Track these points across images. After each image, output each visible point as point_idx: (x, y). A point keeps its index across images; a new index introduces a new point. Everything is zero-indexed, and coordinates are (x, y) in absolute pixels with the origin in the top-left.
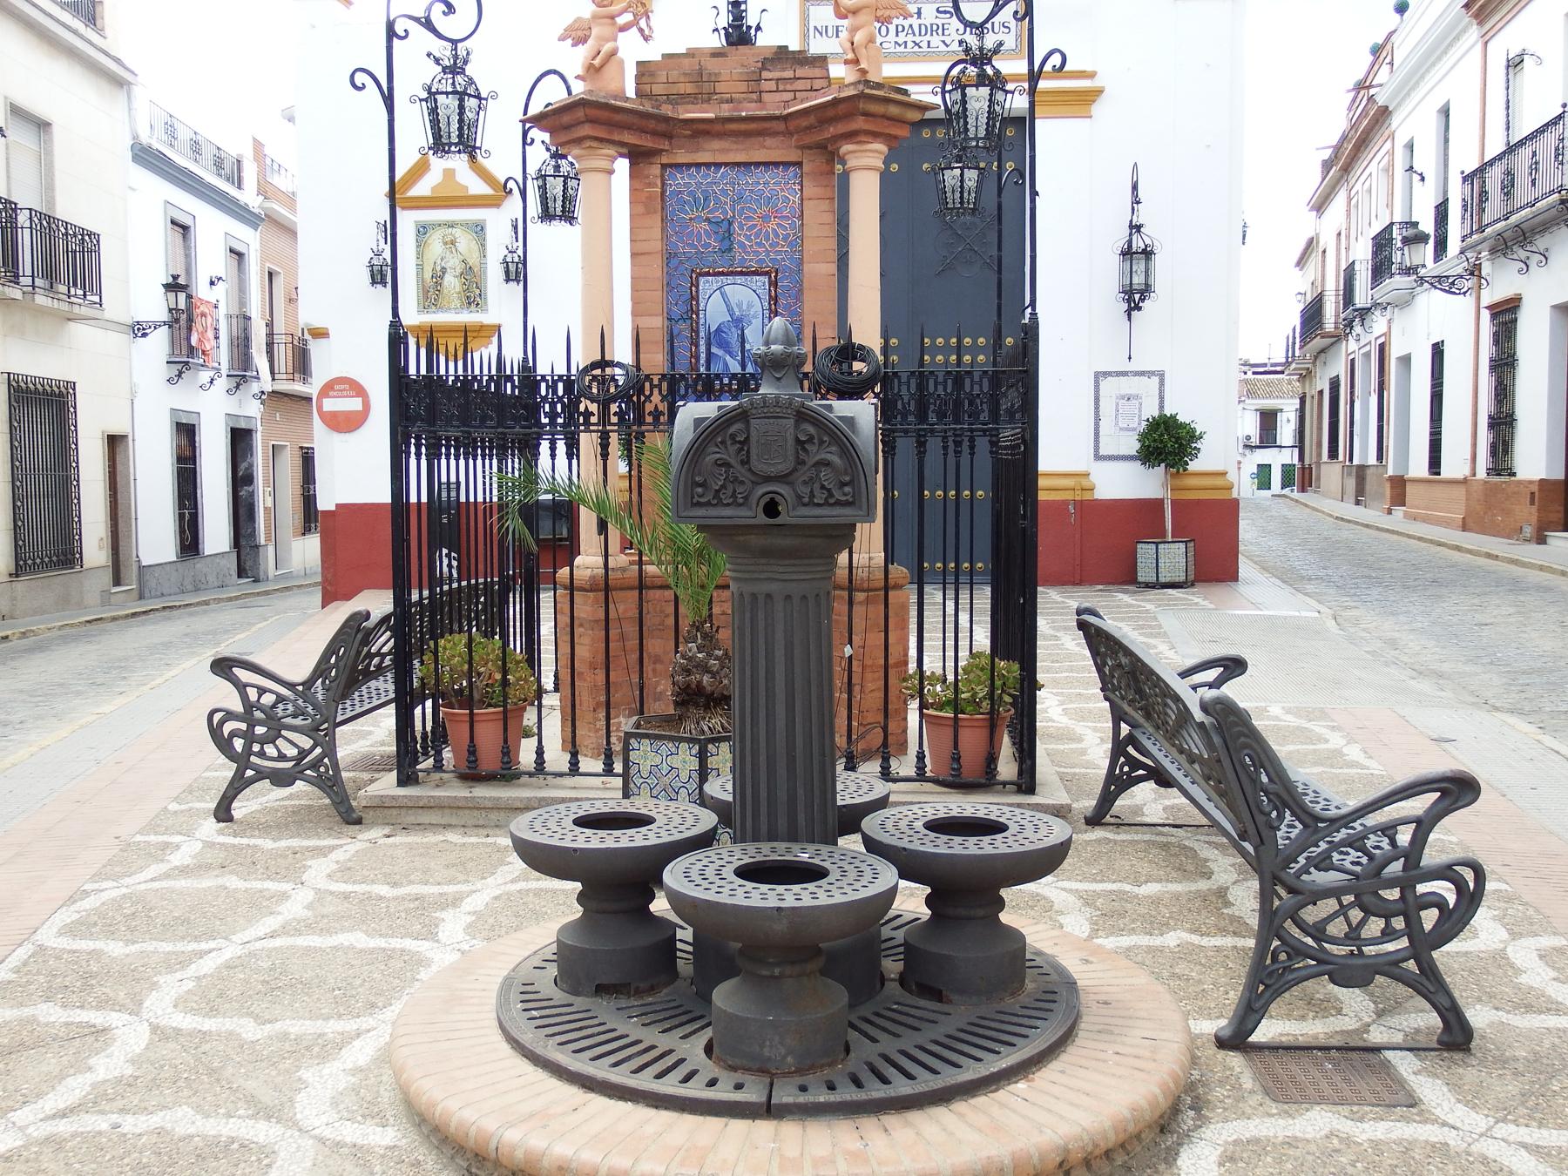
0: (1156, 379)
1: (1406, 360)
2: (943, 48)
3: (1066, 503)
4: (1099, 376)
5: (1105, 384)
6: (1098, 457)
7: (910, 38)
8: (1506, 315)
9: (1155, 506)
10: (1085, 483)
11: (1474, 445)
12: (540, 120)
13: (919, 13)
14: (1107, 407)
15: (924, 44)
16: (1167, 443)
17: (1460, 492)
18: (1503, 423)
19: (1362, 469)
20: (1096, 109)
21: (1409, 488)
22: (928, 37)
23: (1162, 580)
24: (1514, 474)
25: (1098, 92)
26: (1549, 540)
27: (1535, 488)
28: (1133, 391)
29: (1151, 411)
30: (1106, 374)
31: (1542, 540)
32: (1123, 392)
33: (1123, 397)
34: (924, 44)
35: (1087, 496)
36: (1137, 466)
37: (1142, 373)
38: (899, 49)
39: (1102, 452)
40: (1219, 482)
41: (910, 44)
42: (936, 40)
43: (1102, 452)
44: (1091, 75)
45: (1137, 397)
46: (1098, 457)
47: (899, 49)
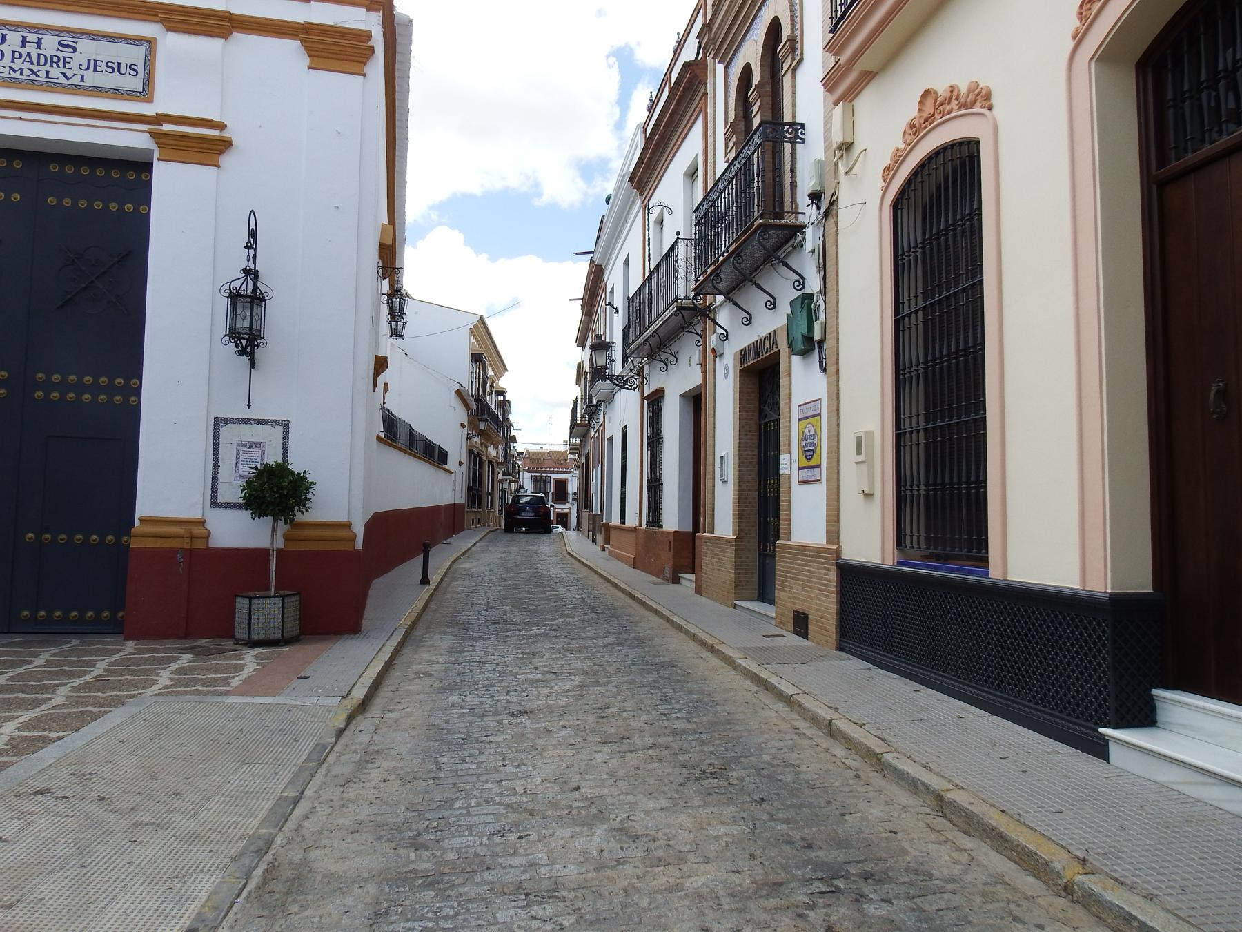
0: (280, 429)
1: (611, 439)
2: (62, 80)
3: (174, 551)
4: (219, 422)
5: (226, 432)
6: (215, 504)
7: (27, 65)
8: (655, 401)
9: (259, 556)
10: (197, 530)
11: (1103, 478)
12: (647, 398)
13: (39, 44)
14: (227, 454)
15: (42, 74)
16: (276, 491)
17: (633, 536)
18: (654, 486)
19: (595, 515)
20: (226, 160)
21: (612, 532)
22: (47, 67)
23: (255, 637)
24: (661, 526)
25: (226, 144)
26: (682, 581)
27: (671, 538)
28: (256, 439)
29: (273, 457)
30: (227, 421)
31: (676, 580)
32: (245, 440)
33: (244, 445)
34: (42, 74)
35: (199, 545)
36: (247, 514)
37: (260, 422)
38: (13, 75)
39: (220, 499)
40: (342, 533)
41: (26, 72)
42: (55, 72)
43: (220, 499)
44: (221, 126)
45: (259, 445)
46: (215, 504)
47: (13, 75)
